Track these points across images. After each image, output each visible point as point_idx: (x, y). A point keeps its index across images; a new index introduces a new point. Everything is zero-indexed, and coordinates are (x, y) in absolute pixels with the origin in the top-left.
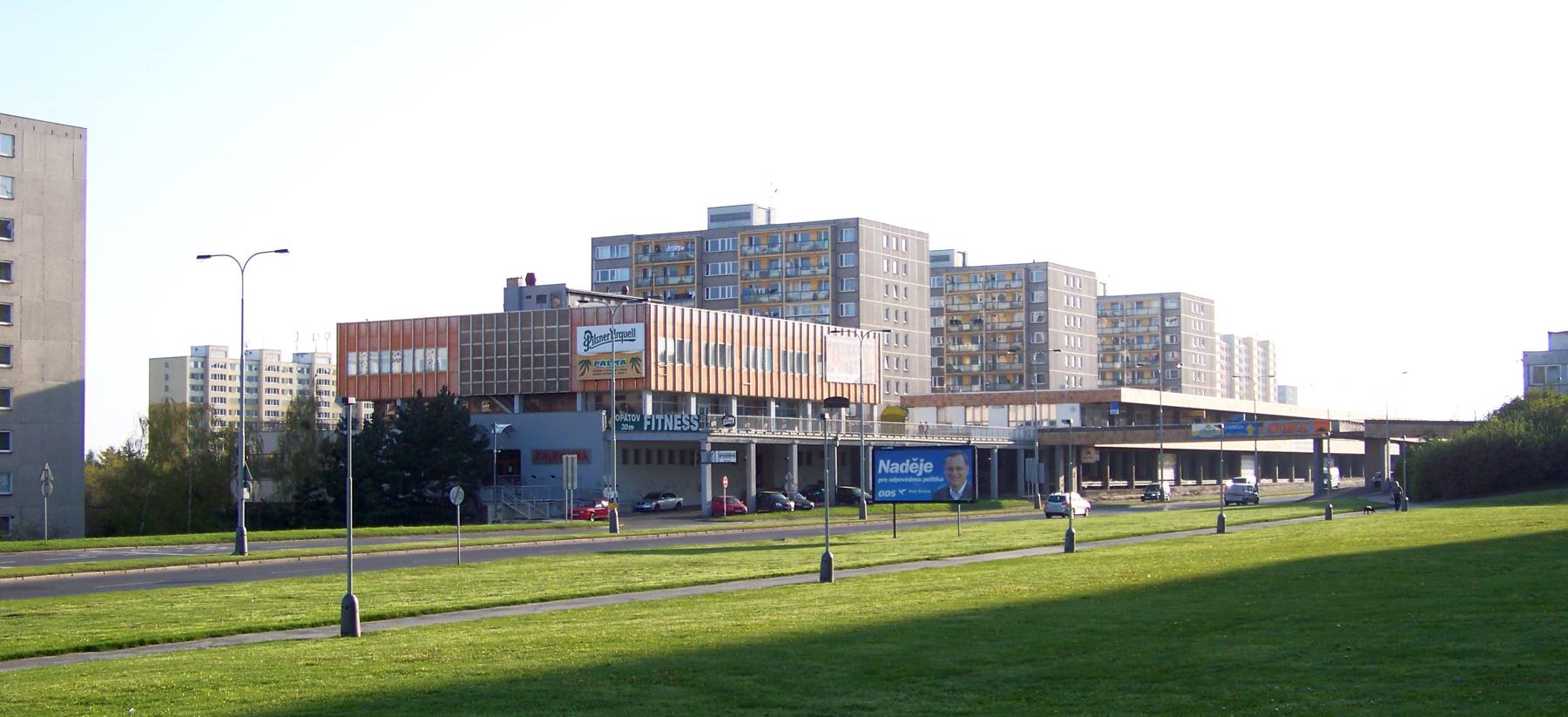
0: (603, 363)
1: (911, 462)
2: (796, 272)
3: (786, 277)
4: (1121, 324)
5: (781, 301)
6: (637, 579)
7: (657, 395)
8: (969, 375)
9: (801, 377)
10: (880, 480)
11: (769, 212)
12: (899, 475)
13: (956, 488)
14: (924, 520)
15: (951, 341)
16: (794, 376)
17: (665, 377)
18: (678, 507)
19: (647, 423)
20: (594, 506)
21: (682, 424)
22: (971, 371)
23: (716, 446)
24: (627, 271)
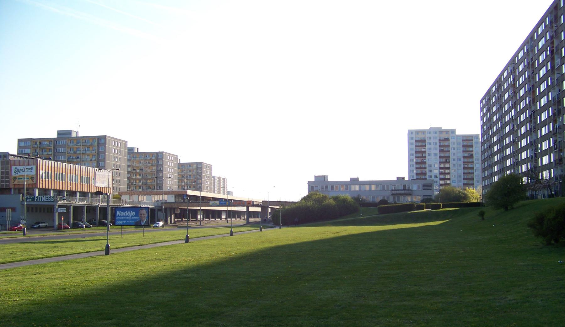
0: (21, 178)
2: (85, 152)
3: (82, 153)
4: (184, 172)
5: (80, 161)
6: (35, 254)
7: (39, 189)
9: (87, 185)
10: (117, 218)
11: (77, 133)
12: (124, 216)
13: (143, 222)
14: (128, 231)
15: (133, 175)
16: (85, 184)
17: (42, 184)
18: (46, 227)
19: (36, 199)
20: (17, 226)
21: (48, 199)
22: (139, 185)
23: (59, 207)
24: (30, 150)
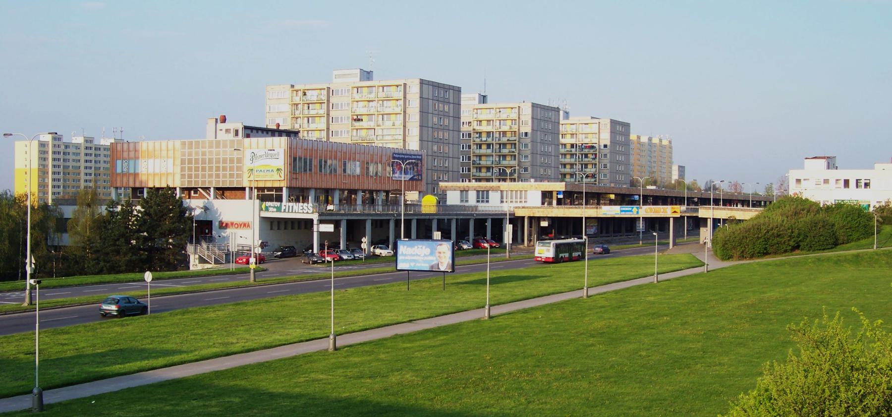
1: (418, 248)
8: (485, 167)
12: (411, 255)
21: (303, 209)
